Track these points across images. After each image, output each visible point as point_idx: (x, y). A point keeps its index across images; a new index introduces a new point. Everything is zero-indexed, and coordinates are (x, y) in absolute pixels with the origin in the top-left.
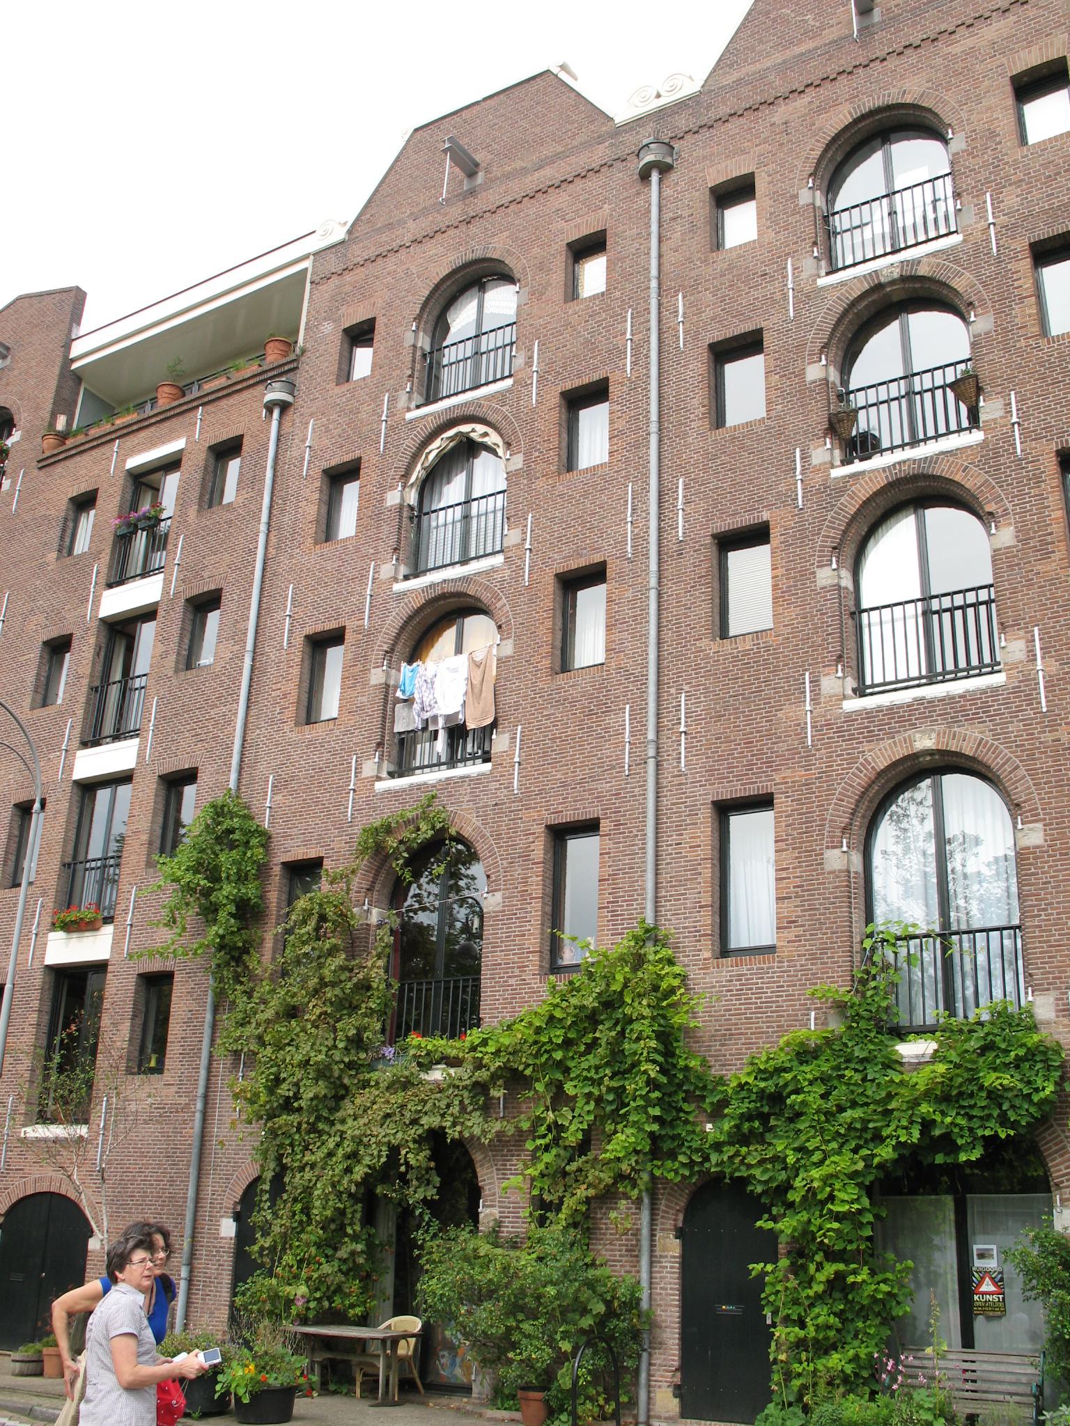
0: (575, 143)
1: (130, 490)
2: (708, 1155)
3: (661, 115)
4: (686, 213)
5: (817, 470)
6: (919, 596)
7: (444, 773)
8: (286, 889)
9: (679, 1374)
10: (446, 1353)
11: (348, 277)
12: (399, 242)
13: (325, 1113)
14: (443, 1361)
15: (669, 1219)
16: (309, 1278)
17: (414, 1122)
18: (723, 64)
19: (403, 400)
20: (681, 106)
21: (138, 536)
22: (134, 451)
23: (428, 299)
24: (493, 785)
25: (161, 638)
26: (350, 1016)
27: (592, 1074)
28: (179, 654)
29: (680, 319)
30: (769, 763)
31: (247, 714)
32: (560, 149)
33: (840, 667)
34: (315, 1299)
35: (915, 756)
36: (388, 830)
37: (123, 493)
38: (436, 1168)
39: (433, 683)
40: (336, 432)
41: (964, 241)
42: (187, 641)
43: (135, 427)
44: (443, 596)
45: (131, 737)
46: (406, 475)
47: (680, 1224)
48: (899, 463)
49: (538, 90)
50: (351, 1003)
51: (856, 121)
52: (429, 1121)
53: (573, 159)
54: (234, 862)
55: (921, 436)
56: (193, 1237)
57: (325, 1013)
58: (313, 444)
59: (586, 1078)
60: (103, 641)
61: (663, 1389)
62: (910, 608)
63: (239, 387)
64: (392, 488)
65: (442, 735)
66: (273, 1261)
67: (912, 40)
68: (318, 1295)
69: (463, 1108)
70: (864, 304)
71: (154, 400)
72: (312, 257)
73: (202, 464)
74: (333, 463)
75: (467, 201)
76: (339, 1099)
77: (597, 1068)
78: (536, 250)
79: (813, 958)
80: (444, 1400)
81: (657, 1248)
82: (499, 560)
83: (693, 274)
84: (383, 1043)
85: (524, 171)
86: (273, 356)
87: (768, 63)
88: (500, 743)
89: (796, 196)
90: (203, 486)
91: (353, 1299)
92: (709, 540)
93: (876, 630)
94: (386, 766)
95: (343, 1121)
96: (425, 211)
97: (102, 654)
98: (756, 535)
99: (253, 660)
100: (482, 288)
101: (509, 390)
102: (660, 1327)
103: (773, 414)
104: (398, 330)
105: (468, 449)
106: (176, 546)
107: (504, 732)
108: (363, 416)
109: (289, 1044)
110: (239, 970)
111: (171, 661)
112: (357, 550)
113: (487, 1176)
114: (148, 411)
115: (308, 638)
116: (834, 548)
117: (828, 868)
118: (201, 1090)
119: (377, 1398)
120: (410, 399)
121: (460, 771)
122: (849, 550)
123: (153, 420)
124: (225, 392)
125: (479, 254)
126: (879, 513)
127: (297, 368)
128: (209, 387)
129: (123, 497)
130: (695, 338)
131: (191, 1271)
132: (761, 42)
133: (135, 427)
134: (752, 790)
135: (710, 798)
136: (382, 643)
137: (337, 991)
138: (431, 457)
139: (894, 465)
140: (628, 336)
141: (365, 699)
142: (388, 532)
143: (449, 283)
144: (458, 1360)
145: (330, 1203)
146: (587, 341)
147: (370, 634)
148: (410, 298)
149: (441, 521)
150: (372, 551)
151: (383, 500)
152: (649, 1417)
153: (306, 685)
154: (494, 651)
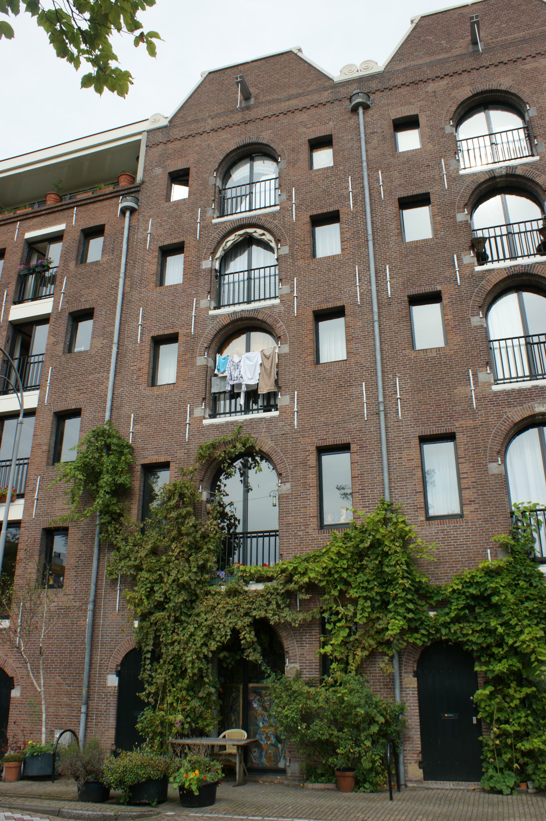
0: (309, 89)
1: (26, 250)
2: (440, 630)
3: (361, 80)
4: (379, 131)
5: (467, 266)
6: (523, 335)
7: (241, 418)
8: (143, 480)
9: (420, 755)
10: (256, 750)
11: (170, 146)
12: (202, 129)
13: (185, 610)
14: (255, 754)
15: (409, 666)
16: (183, 710)
17: (247, 614)
18: (394, 60)
19: (210, 213)
20: (372, 77)
21: (33, 276)
22: (30, 229)
23: (223, 161)
24: (280, 424)
25: (52, 333)
26: (196, 553)
27: (366, 584)
28: (65, 343)
29: (381, 184)
30: (451, 417)
31: (115, 379)
32: (300, 91)
33: (488, 368)
34: (187, 722)
35: (534, 416)
36: (214, 446)
37: (23, 252)
38: (258, 641)
39: (238, 365)
40: (167, 227)
41: (540, 160)
42: (69, 336)
43: (31, 216)
44: (241, 319)
45: (34, 390)
46: (214, 253)
47: (415, 669)
48: (514, 266)
49: (285, 60)
50: (196, 546)
51: (474, 96)
52: (258, 614)
53: (309, 97)
54: (112, 462)
55: (252, 299)
56: (89, 687)
57: (183, 551)
58: (152, 231)
59: (363, 588)
60: (11, 334)
61: (413, 764)
62: (516, 341)
63: (101, 198)
64: (205, 259)
65: (242, 395)
66: (156, 701)
67: (502, 60)
68: (189, 720)
69: (278, 606)
70: (485, 186)
71: (45, 202)
72: (146, 133)
73: (77, 238)
74: (166, 243)
75: (245, 112)
76: (192, 601)
77: (368, 581)
78: (289, 141)
79: (486, 521)
80: (265, 778)
81: (403, 683)
82: (277, 301)
83: (386, 162)
84: (218, 569)
85: (279, 100)
86: (124, 183)
87: (421, 62)
88: (283, 400)
89: (444, 129)
90: (78, 251)
91: (208, 721)
92: (406, 298)
93: (497, 352)
94: (208, 412)
95: (198, 615)
96: (218, 115)
97: (10, 342)
98: (172, 338)
99: (118, 348)
100: (252, 159)
101: (277, 212)
102: (408, 728)
103: (439, 236)
104: (205, 176)
105: (249, 242)
106: (62, 283)
107: (286, 395)
108: (184, 219)
109: (159, 570)
110: (117, 526)
111: (60, 347)
112: (184, 291)
113: (291, 646)
114: (36, 208)
115: (153, 338)
116: (480, 307)
117: (491, 472)
118: (92, 598)
119: (235, 780)
120: (214, 213)
121: (250, 416)
122: (485, 308)
123: (44, 212)
124: (92, 200)
125: (254, 140)
126: (499, 291)
127: (140, 191)
128: (80, 197)
129: (23, 254)
130: (390, 193)
131: (87, 708)
132: (416, 51)
133: (31, 216)
134: (442, 430)
135: (418, 434)
136: (203, 342)
137: (190, 539)
138: (229, 244)
139: (511, 267)
140: (350, 190)
141: (194, 373)
142: (204, 283)
143: (234, 154)
144: (264, 753)
145: (196, 665)
146: (324, 191)
147: (195, 337)
148: (211, 159)
149: (231, 280)
150: (194, 292)
151: (199, 265)
152: (406, 781)
153: (151, 364)
154: (277, 351)
